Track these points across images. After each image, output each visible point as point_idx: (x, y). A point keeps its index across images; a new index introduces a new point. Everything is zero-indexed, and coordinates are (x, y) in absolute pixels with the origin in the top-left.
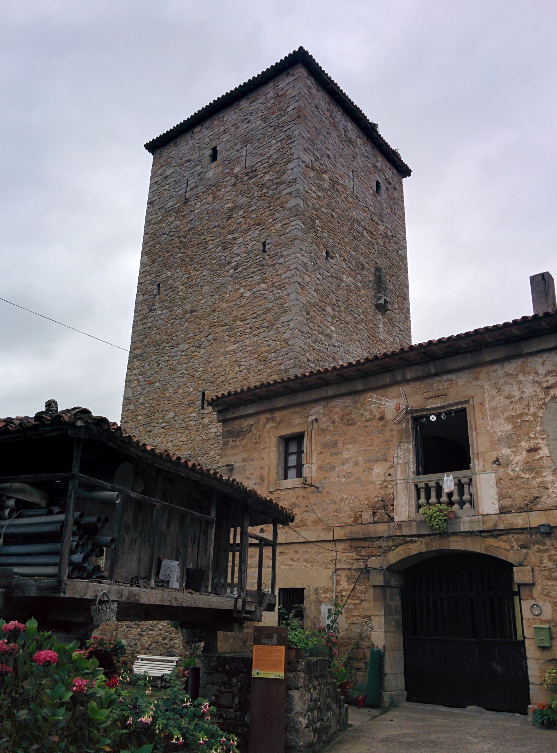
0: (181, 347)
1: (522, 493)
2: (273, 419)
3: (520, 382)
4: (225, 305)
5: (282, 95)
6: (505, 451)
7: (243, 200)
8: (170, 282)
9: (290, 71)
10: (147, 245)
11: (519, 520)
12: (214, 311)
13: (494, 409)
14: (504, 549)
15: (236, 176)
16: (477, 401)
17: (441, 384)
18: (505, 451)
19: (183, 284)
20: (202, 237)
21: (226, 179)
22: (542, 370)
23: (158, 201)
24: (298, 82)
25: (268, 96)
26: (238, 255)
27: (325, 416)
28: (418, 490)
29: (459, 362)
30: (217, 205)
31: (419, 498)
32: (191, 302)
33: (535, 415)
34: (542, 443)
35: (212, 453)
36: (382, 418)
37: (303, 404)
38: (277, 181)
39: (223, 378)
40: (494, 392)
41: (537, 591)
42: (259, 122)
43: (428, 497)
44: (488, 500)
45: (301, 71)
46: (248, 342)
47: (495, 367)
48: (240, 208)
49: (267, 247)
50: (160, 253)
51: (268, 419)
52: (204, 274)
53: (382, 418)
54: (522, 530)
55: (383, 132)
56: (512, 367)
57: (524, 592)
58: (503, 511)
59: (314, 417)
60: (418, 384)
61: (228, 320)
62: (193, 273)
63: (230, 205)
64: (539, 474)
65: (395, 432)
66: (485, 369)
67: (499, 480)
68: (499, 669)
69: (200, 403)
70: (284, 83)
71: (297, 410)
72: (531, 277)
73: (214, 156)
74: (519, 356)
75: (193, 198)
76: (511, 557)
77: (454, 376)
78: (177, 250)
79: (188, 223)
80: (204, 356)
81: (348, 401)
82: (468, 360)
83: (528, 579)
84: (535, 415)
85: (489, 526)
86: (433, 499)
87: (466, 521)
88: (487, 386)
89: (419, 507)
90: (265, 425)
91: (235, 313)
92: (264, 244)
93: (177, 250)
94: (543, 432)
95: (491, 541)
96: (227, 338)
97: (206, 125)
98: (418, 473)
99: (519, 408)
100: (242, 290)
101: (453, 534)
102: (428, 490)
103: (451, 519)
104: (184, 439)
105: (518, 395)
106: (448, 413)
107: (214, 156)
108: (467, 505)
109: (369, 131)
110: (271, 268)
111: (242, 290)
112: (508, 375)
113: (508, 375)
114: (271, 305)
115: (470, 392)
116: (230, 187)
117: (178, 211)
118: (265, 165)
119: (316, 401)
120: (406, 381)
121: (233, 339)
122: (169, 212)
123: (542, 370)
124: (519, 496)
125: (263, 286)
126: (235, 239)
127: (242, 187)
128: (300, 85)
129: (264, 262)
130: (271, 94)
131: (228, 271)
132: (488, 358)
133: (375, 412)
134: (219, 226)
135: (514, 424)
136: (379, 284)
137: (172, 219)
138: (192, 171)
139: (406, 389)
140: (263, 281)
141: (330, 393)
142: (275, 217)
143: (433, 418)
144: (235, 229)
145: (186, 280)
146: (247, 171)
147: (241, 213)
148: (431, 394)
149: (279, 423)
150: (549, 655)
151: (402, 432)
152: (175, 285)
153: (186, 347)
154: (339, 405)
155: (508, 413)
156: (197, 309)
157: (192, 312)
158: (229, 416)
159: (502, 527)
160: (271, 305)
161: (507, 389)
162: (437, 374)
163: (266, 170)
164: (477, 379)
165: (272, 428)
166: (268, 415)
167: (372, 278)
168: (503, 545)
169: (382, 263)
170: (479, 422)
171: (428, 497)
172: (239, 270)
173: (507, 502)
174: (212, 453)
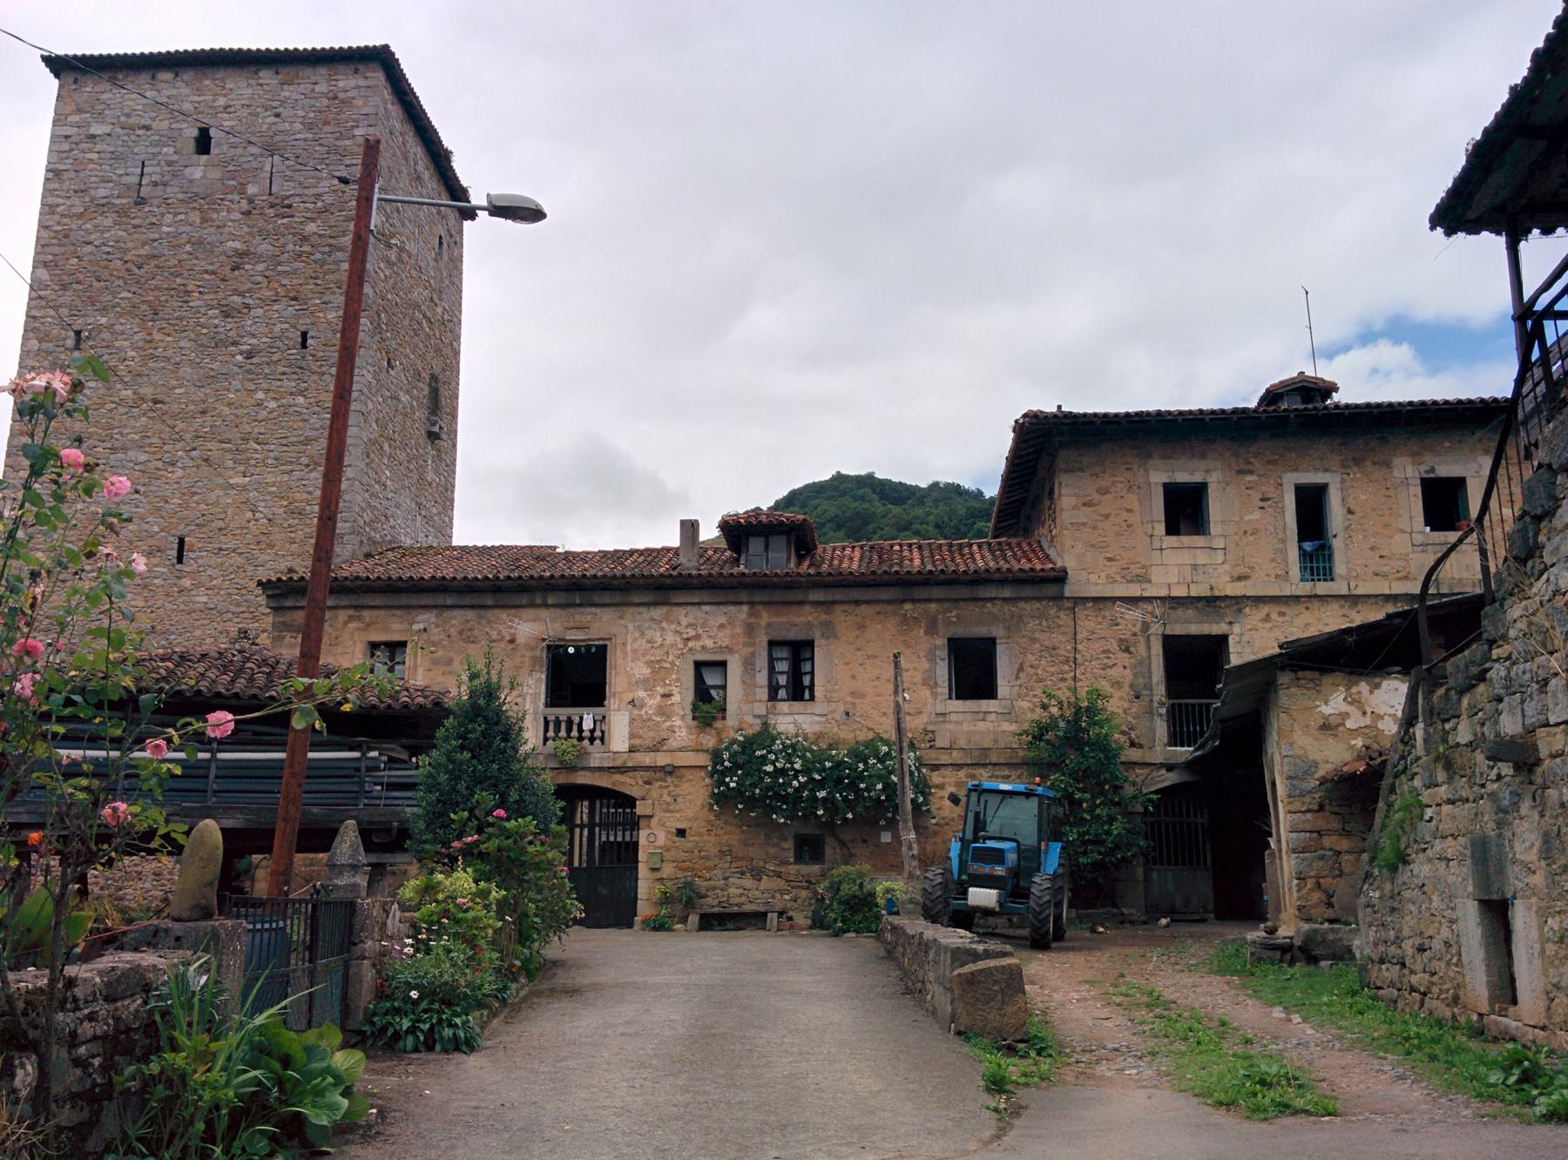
0: (132, 454)
1: (652, 734)
2: (359, 618)
3: (663, 629)
4: (227, 410)
5: (343, 102)
6: (641, 694)
7: (264, 248)
8: (106, 335)
9: (361, 67)
10: (48, 250)
11: (646, 759)
12: (204, 412)
13: (635, 651)
14: (628, 785)
15: (251, 201)
16: (619, 640)
17: (585, 615)
18: (641, 694)
19: (136, 349)
20: (178, 280)
21: (229, 197)
22: (684, 622)
23: (72, 174)
24: (367, 88)
25: (317, 88)
26: (253, 336)
27: (437, 626)
28: (547, 722)
29: (607, 598)
30: (209, 234)
31: (546, 730)
32: (154, 385)
33: (672, 663)
34: (675, 691)
35: (198, 633)
36: (512, 641)
37: (408, 607)
38: (331, 241)
39: (221, 524)
40: (637, 634)
41: (654, 822)
42: (298, 126)
43: (557, 730)
44: (619, 741)
45: (378, 77)
46: (270, 479)
47: (641, 609)
48: (259, 259)
49: (310, 341)
50: (81, 277)
51: (350, 617)
52: (182, 344)
53: (512, 641)
54: (648, 768)
55: (459, 166)
56: (657, 612)
57: (643, 823)
58: (632, 750)
59: (421, 626)
60: (558, 611)
61: (234, 434)
62: (157, 336)
63: (238, 245)
64: (669, 718)
65: (527, 660)
66: (631, 610)
67: (632, 721)
68: (605, 892)
69: (174, 553)
70: (347, 82)
71: (398, 612)
72: (386, 47)
73: (203, 143)
74: (665, 604)
75: (156, 202)
76: (635, 792)
77: (598, 610)
78: (121, 282)
79: (144, 244)
80: (183, 481)
81: (470, 614)
82: (617, 598)
83: (648, 812)
84: (672, 663)
85: (618, 763)
86: (563, 733)
87: (597, 757)
88: (631, 627)
89: (546, 739)
90: (346, 623)
91: (247, 428)
92: (304, 335)
93: (121, 282)
94: (678, 680)
95: (618, 777)
96: (230, 463)
97: (185, 77)
98: (547, 705)
99: (658, 655)
100: (260, 395)
101: (582, 769)
102: (558, 723)
103: (584, 754)
104: (141, 604)
105: (659, 641)
106: (588, 648)
107: (203, 143)
108: (598, 742)
109: (439, 158)
110: (315, 377)
111: (260, 395)
112: (652, 619)
113: (652, 619)
114: (315, 433)
115: (614, 630)
116: (239, 216)
117: (122, 213)
118: (310, 206)
119: (426, 607)
120: (546, 606)
121: (242, 468)
122: (103, 207)
123: (684, 622)
124: (649, 737)
125: (301, 400)
126: (247, 306)
127: (261, 223)
128: (376, 100)
129: (304, 364)
130: (322, 88)
131: (233, 356)
132: (636, 600)
133: (504, 632)
134: (213, 273)
135: (653, 669)
136: (435, 395)
137: (109, 222)
138: (156, 150)
139: (545, 613)
140: (301, 393)
141: (449, 602)
142: (326, 298)
143: (571, 650)
144: (249, 291)
145: (141, 344)
146: (272, 199)
147: (260, 267)
148: (572, 624)
149: (368, 625)
150: (658, 875)
151: (534, 660)
152: (117, 344)
153: (143, 458)
154: (457, 618)
155: (648, 657)
156: (167, 400)
157: (156, 402)
158: (289, 603)
159: (630, 764)
160: (315, 433)
161: (649, 634)
162: (580, 605)
163: (309, 215)
164: (622, 618)
165: (357, 629)
166: (351, 612)
167: (426, 391)
168: (629, 780)
169: (437, 366)
170: (620, 661)
171: (557, 730)
172: (254, 360)
173: (637, 742)
174: (198, 633)
